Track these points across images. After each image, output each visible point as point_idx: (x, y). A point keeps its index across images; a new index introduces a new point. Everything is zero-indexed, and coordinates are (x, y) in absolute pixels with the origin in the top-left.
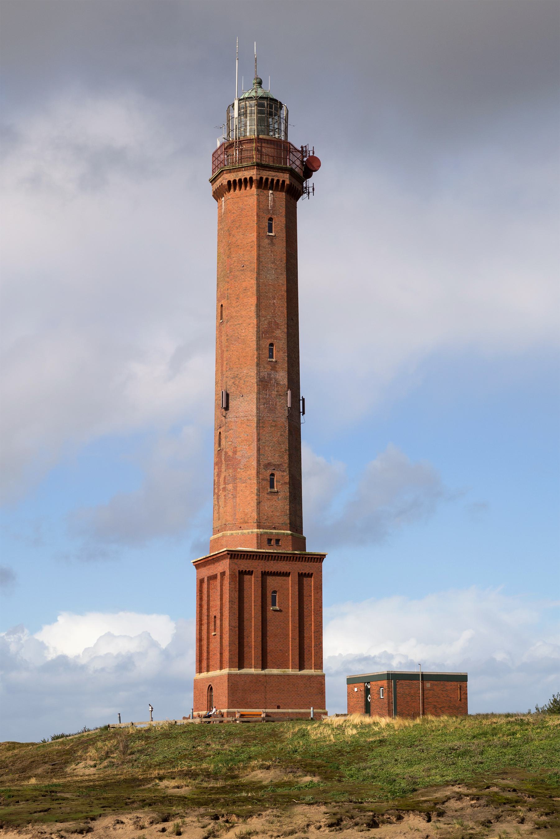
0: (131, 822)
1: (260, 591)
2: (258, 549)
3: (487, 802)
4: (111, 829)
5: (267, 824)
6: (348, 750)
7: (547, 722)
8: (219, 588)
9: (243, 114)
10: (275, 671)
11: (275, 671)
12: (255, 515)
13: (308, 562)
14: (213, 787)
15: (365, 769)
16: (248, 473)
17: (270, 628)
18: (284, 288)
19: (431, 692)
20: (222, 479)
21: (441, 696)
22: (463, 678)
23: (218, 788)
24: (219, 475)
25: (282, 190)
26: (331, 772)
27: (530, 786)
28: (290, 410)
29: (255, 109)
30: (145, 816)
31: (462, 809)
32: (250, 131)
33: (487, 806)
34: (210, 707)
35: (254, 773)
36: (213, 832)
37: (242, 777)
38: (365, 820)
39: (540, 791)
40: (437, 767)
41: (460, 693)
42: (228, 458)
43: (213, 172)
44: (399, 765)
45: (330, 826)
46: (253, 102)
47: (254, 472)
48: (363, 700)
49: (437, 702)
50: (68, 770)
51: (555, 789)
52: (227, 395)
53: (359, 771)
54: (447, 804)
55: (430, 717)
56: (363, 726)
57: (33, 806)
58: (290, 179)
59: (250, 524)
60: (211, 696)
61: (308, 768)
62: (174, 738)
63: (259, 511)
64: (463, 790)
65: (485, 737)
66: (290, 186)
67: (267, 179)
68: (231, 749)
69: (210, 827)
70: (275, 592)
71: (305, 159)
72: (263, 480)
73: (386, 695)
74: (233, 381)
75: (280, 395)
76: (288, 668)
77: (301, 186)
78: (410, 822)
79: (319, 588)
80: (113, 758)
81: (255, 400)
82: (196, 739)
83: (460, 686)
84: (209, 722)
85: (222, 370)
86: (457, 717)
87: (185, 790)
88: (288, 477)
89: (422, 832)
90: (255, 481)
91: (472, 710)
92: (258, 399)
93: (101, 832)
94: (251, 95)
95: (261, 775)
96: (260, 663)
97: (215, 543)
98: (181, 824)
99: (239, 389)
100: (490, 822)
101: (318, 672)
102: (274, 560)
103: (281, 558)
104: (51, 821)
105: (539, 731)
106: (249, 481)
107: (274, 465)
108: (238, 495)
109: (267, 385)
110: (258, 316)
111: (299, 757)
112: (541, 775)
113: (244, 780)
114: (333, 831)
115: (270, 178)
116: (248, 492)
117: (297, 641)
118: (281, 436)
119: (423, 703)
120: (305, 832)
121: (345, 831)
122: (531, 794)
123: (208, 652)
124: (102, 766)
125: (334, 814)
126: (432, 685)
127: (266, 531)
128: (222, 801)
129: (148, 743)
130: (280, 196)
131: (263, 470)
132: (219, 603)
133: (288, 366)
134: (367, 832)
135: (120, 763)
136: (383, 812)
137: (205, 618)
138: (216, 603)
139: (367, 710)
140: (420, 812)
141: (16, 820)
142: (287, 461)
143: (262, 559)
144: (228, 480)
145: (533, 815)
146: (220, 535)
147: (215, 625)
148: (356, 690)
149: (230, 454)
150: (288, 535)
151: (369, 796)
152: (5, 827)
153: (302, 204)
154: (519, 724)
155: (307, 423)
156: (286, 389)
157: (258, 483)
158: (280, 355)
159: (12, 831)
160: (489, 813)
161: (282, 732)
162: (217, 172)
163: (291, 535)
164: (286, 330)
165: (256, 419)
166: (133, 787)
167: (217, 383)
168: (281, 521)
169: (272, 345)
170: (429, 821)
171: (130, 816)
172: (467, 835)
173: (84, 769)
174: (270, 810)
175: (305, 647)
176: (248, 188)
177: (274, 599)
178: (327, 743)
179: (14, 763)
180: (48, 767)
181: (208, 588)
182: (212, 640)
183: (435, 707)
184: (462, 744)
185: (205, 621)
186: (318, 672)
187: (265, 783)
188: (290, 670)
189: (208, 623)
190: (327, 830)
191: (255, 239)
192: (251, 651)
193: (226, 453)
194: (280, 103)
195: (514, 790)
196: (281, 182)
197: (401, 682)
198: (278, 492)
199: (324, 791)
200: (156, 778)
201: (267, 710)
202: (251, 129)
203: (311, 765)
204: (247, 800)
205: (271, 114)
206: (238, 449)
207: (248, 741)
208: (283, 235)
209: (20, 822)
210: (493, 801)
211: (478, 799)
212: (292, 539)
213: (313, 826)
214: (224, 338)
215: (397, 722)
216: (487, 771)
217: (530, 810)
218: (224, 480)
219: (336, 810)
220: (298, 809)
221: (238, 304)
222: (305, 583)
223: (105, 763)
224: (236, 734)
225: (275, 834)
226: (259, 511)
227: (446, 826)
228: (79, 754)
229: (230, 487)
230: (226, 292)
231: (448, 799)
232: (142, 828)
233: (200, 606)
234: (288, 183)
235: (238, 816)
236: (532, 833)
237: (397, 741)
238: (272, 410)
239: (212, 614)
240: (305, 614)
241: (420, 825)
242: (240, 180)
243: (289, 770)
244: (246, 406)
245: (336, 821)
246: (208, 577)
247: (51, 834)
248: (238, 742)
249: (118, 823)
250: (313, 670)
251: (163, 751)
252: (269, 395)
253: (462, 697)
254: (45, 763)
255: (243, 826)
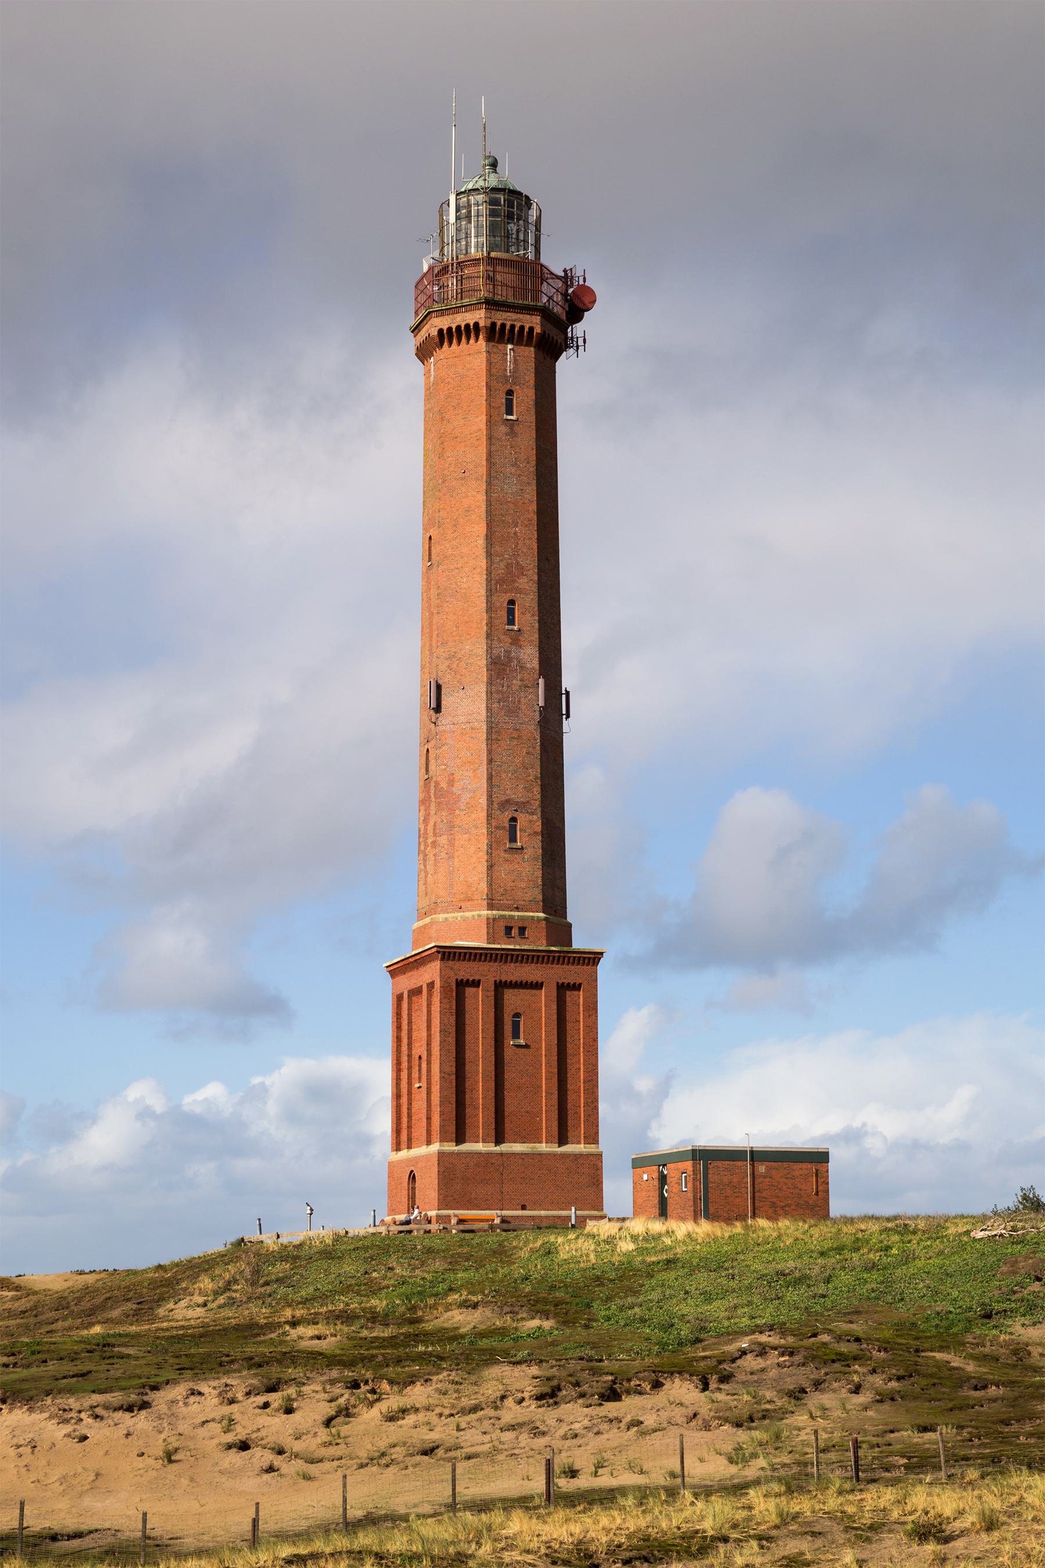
0: (215, 1392)
1: (493, 1014)
2: (489, 943)
3: (805, 1358)
4: (181, 1403)
5: (437, 1396)
6: (612, 1275)
7: (947, 1229)
8: (425, 1009)
9: (464, 215)
10: (518, 1148)
11: (518, 1148)
12: (484, 886)
13: (573, 964)
14: (376, 1338)
15: (631, 1308)
16: (473, 816)
17: (509, 1076)
18: (533, 507)
19: (767, 1180)
20: (430, 828)
21: (785, 1187)
22: (821, 1158)
23: (384, 1339)
24: (426, 821)
25: (528, 344)
26: (576, 1312)
27: (888, 1334)
28: (544, 710)
29: (483, 208)
30: (238, 1383)
31: (763, 1370)
32: (477, 246)
33: (804, 1365)
34: (412, 1204)
35: (449, 1313)
36: (347, 1409)
37: (428, 1321)
38: (598, 1388)
39: (904, 1341)
40: (750, 1303)
41: (817, 1181)
42: (440, 793)
43: (416, 313)
44: (689, 1301)
45: (540, 1397)
46: (481, 198)
47: (483, 815)
48: (657, 1195)
49: (778, 1197)
50: (161, 1312)
51: (930, 1337)
52: (439, 688)
53: (621, 1310)
54: (739, 1362)
55: (762, 1222)
56: (649, 1237)
57: (68, 1368)
58: (542, 325)
59: (476, 902)
60: (414, 1189)
61: (540, 1307)
62: (339, 1257)
63: (491, 880)
64: (773, 1339)
65: (840, 1254)
66: (543, 336)
67: (503, 326)
68: (426, 1275)
69: (342, 1401)
70: (517, 1015)
71: (570, 291)
72: (497, 828)
73: (690, 1185)
74: (447, 663)
75: (526, 686)
76: (541, 1142)
77: (563, 337)
78: (673, 1391)
79: (592, 1008)
80: (235, 1291)
81: (484, 696)
82: (372, 1260)
83: (817, 1170)
84: (410, 1232)
85: (431, 645)
86: (805, 1222)
87: (329, 1343)
88: (539, 823)
89: (687, 1407)
90: (485, 831)
91: (837, 1207)
92: (489, 694)
93: (163, 1408)
94: (477, 186)
95: (460, 1317)
96: (493, 1133)
97: (420, 934)
98: (294, 1396)
99: (458, 677)
100: (803, 1391)
101: (591, 1149)
102: (516, 962)
103: (528, 959)
104: (85, 1391)
105: (929, 1243)
106: (474, 831)
107: (517, 804)
108: (456, 854)
109: (505, 670)
110: (489, 555)
111: (528, 1289)
112: (915, 1315)
113: (428, 1326)
114: (543, 1406)
115: (508, 324)
116: (472, 849)
117: (556, 1096)
118: (526, 757)
119: (753, 1198)
120: (496, 1408)
121: (563, 1406)
122: (884, 1345)
123: (410, 1116)
124: (215, 1305)
125: (548, 1379)
126: (768, 1169)
127: (503, 913)
128: (380, 1358)
129: (295, 1267)
130: (527, 353)
131: (498, 812)
132: (424, 1034)
133: (540, 638)
134: (598, 1408)
135: (245, 1299)
136: (631, 1375)
137: (404, 1059)
138: (420, 1034)
139: (663, 1212)
140: (691, 1375)
141: (28, 1390)
142: (539, 796)
143: (495, 961)
144: (440, 829)
145: (878, 1380)
146: (427, 920)
147: (420, 1070)
148: (645, 1177)
149: (444, 785)
150: (539, 920)
151: (623, 1351)
152: (9, 1401)
153: (565, 365)
154: (899, 1233)
155: (576, 734)
156: (536, 676)
157: (490, 833)
158: (527, 619)
159: (21, 1408)
160: (802, 1376)
161: (515, 1248)
162: (421, 316)
163: (546, 919)
164: (536, 578)
165: (485, 727)
166: (245, 1338)
167: (423, 667)
168: (528, 897)
169: (512, 602)
170: (705, 1388)
171: (215, 1383)
172: (758, 1411)
173: (185, 1312)
174: (445, 1374)
175: (569, 1106)
176: (472, 341)
177: (516, 1027)
178: (582, 1265)
179: (79, 1300)
180: (131, 1306)
181: (410, 1009)
182: (415, 1096)
183: (773, 1205)
184: (799, 1266)
185: (405, 1065)
186: (591, 1149)
187: (462, 1331)
188: (544, 1145)
189: (410, 1068)
190: (534, 1404)
191: (483, 426)
192: (478, 1115)
193: (437, 783)
194: (527, 197)
195: (858, 1340)
196: (526, 330)
197: (715, 1163)
198: (522, 848)
199: (553, 1344)
200: (286, 1322)
201: (505, 1213)
202: (476, 245)
203: (546, 1301)
204: (421, 1358)
205: (510, 216)
206: (457, 776)
207: (457, 1262)
208: (532, 418)
209: (31, 1393)
210: (819, 1357)
211: (791, 1354)
212: (547, 928)
213: (510, 1399)
214: (433, 592)
215: (704, 1228)
216: (828, 1310)
217: (874, 1371)
218: (434, 829)
219: (554, 1371)
220: (495, 1371)
221: (456, 534)
222: (568, 999)
223: (221, 1300)
224: (438, 1251)
225: (447, 1412)
226: (491, 880)
227: (729, 1397)
228: (184, 1285)
229: (443, 840)
230: (437, 515)
231: (744, 1353)
232: (232, 1401)
233: (398, 1039)
234: (539, 331)
235: (391, 1382)
236: (866, 1409)
237: (695, 1261)
238: (513, 711)
239: (416, 1053)
240: (569, 1051)
241: (687, 1396)
242: (458, 327)
243: (506, 1309)
244: (469, 705)
245: (549, 1391)
246: (409, 991)
247: (80, 1412)
248: (439, 1265)
249: (193, 1394)
250: (582, 1145)
251: (318, 1279)
252: (508, 686)
253: (820, 1188)
254: (128, 1300)
255: (397, 1398)
